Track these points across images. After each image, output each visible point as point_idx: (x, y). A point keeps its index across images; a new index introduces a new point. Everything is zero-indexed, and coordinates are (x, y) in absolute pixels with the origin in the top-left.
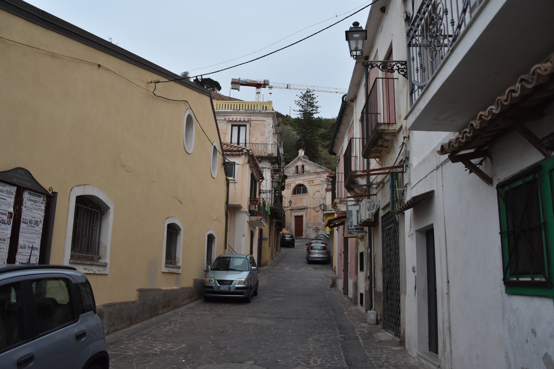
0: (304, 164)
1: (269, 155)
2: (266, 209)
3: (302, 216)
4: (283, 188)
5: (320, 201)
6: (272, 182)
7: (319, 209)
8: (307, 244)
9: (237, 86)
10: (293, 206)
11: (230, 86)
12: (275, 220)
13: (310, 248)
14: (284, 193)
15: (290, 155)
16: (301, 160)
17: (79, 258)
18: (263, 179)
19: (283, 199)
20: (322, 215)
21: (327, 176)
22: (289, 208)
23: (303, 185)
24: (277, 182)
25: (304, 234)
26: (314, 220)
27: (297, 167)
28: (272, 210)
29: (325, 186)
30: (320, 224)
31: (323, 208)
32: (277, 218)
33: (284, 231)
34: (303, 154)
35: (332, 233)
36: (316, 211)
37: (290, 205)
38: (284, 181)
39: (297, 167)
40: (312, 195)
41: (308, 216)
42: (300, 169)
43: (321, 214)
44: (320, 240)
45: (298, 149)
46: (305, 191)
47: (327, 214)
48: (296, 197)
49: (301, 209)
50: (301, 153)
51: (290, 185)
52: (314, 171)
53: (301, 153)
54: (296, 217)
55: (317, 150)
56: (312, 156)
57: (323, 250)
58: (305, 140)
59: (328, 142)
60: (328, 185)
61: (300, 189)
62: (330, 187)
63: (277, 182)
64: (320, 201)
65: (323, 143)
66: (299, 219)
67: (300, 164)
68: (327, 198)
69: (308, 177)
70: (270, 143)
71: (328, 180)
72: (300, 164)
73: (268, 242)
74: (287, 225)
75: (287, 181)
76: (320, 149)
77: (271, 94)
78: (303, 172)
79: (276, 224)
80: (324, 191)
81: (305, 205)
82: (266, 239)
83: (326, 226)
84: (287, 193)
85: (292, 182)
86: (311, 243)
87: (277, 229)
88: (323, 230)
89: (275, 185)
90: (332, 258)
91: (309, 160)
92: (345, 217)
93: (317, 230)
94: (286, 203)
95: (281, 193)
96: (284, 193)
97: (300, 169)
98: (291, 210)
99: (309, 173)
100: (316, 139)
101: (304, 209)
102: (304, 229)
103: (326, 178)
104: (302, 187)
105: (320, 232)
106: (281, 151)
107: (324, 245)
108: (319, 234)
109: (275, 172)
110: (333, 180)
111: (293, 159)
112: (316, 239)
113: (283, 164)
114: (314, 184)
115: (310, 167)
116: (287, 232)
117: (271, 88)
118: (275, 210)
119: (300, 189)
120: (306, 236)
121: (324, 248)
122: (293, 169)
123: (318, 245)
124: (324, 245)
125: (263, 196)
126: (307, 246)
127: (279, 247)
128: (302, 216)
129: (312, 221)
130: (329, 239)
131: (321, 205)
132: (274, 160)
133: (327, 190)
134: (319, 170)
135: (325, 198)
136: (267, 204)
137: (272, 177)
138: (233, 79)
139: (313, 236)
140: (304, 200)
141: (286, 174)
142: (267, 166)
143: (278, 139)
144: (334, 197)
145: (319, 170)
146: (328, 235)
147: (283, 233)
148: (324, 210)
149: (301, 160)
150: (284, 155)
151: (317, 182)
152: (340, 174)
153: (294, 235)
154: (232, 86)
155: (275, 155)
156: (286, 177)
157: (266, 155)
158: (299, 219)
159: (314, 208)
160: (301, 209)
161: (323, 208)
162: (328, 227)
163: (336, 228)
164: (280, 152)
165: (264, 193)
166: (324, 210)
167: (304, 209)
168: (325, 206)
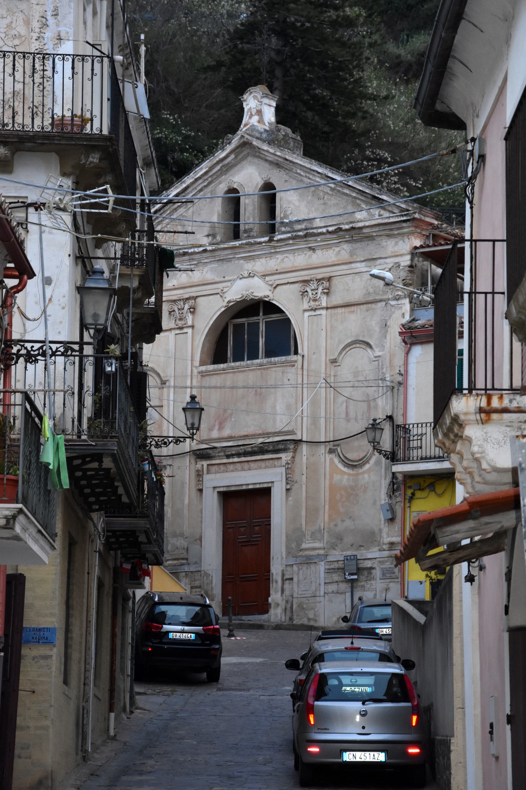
0: (278, 178)
1: (59, 123)
2: (48, 456)
3: (264, 493)
4: (149, 327)
5: (369, 402)
6: (81, 290)
7: (360, 448)
8: (292, 665)
10: (209, 432)
12: (99, 520)
13: (312, 688)
14: (152, 354)
15: (188, 127)
16: (257, 153)
18: (24, 271)
19: (153, 394)
20: (385, 483)
21: (414, 252)
22: (187, 446)
23: (270, 308)
24: (111, 292)
25: (275, 597)
26: (331, 513)
27: (233, 201)
28: (79, 459)
29: (402, 312)
30: (370, 538)
31: (386, 441)
32: (114, 507)
33: (159, 582)
34: (270, 115)
35: (442, 590)
37: (194, 428)
38: (152, 283)
39: (233, 201)
40: (320, 363)
41: (301, 491)
42: (250, 212)
43: (375, 477)
44: (371, 634)
45: (241, 87)
46: (281, 340)
47: (410, 477)
48: (228, 379)
49: (262, 450)
50: (259, 109)
51: (191, 303)
52: (332, 224)
53: (259, 109)
54: (228, 497)
55: (354, 94)
56: (324, 130)
57: (390, 697)
58: (283, 31)
59: (421, 41)
60: (417, 305)
61: (252, 332)
62: (427, 317)
63: (111, 292)
64: (369, 402)
65: (391, 48)
66: (245, 510)
67: (248, 177)
68: (412, 381)
69: (300, 259)
70: (67, 48)
71: (416, 277)
72: (248, 177)
73: (56, 652)
74: (172, 543)
75: (174, 282)
76: (373, 85)
78: (272, 229)
79: (108, 546)
80: (394, 338)
81: (281, 423)
82: (43, 637)
83: (400, 560)
84: (172, 357)
85: (203, 290)
86: (320, 658)
87: (117, 573)
88: (386, 575)
89: (102, 310)
90: (446, 745)
91: (308, 154)
92: (513, 502)
93: (354, 573)
94: (165, 414)
95: (137, 357)
96: (152, 354)
97: (250, 212)
98: (200, 455)
99: (306, 235)
100: (350, 23)
101: (278, 448)
102: (276, 568)
103: (406, 261)
104: (262, 321)
105: (374, 590)
106: (137, 98)
107: (394, 669)
108: (368, 596)
109: (94, 228)
110: (442, 272)
111: (212, 150)
112: (353, 628)
113: (146, 179)
114: (337, 299)
115: (310, 195)
116: (177, 590)
118: (98, 457)
119: (252, 332)
120: (289, 609)
121: (397, 689)
122: (210, 211)
123: (357, 671)
124: (394, 669)
125: (27, 376)
126: (293, 675)
127: (124, 683)
128: (264, 493)
129: (324, 519)
130: (422, 630)
131: (375, 426)
132: (94, 158)
133: (411, 336)
134: (365, 216)
135: (399, 386)
136: (48, 424)
137: (82, 259)
139: (330, 610)
140: (274, 398)
141: (164, 240)
142: (50, 197)
143: (111, 27)
144: (446, 386)
145: (365, 216)
146: (418, 604)
147: (148, 598)
148: (393, 457)
149: (257, 153)
150: (155, 121)
151: (352, 285)
152: (484, 249)
153: (216, 608)
155: (100, 124)
156: (165, 260)
157: (42, 123)
158: (245, 510)
159: (334, 446)
160: (262, 450)
161: (386, 443)
162: (412, 564)
163: (462, 569)
164: (129, 104)
165: (30, 358)
166: (393, 457)
167: (278, 448)
168: (400, 432)
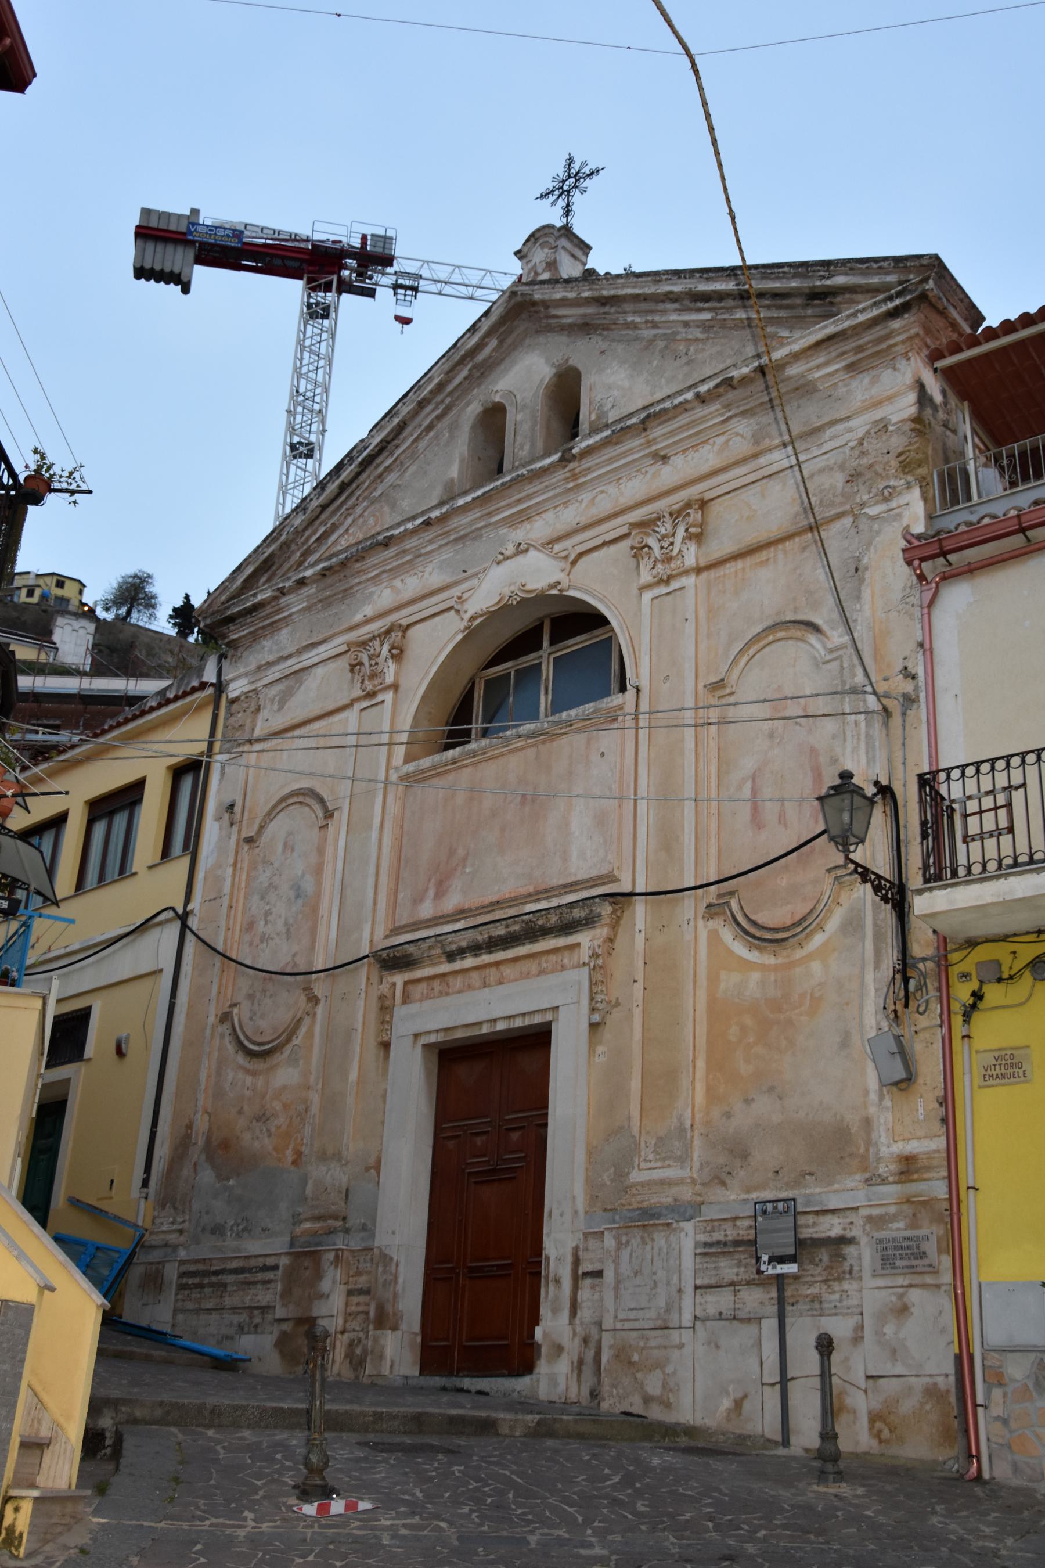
3: (534, 1041)
9: (175, 258)
11: (127, 250)
17: (118, 1355)
25: (553, 1326)
30: (837, 1146)
36: (757, 935)
41: (632, 1028)
49: (532, 932)
54: (459, 1061)
57: (234, 640)
77: (405, 321)
102: (559, 1241)
114: (719, 546)
117: (408, 287)
120: (589, 1362)
128: (534, 1041)
138: (146, 212)
140: (581, 800)
154: (140, 254)
